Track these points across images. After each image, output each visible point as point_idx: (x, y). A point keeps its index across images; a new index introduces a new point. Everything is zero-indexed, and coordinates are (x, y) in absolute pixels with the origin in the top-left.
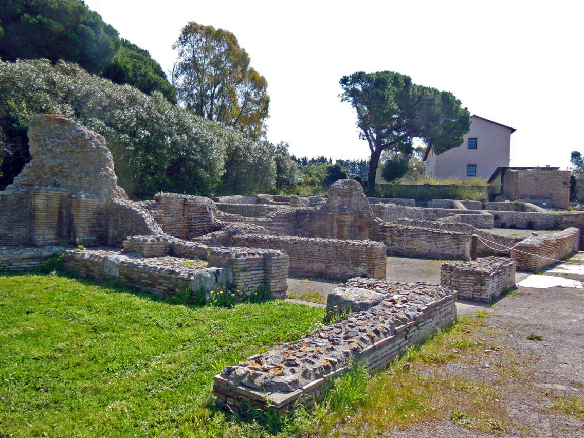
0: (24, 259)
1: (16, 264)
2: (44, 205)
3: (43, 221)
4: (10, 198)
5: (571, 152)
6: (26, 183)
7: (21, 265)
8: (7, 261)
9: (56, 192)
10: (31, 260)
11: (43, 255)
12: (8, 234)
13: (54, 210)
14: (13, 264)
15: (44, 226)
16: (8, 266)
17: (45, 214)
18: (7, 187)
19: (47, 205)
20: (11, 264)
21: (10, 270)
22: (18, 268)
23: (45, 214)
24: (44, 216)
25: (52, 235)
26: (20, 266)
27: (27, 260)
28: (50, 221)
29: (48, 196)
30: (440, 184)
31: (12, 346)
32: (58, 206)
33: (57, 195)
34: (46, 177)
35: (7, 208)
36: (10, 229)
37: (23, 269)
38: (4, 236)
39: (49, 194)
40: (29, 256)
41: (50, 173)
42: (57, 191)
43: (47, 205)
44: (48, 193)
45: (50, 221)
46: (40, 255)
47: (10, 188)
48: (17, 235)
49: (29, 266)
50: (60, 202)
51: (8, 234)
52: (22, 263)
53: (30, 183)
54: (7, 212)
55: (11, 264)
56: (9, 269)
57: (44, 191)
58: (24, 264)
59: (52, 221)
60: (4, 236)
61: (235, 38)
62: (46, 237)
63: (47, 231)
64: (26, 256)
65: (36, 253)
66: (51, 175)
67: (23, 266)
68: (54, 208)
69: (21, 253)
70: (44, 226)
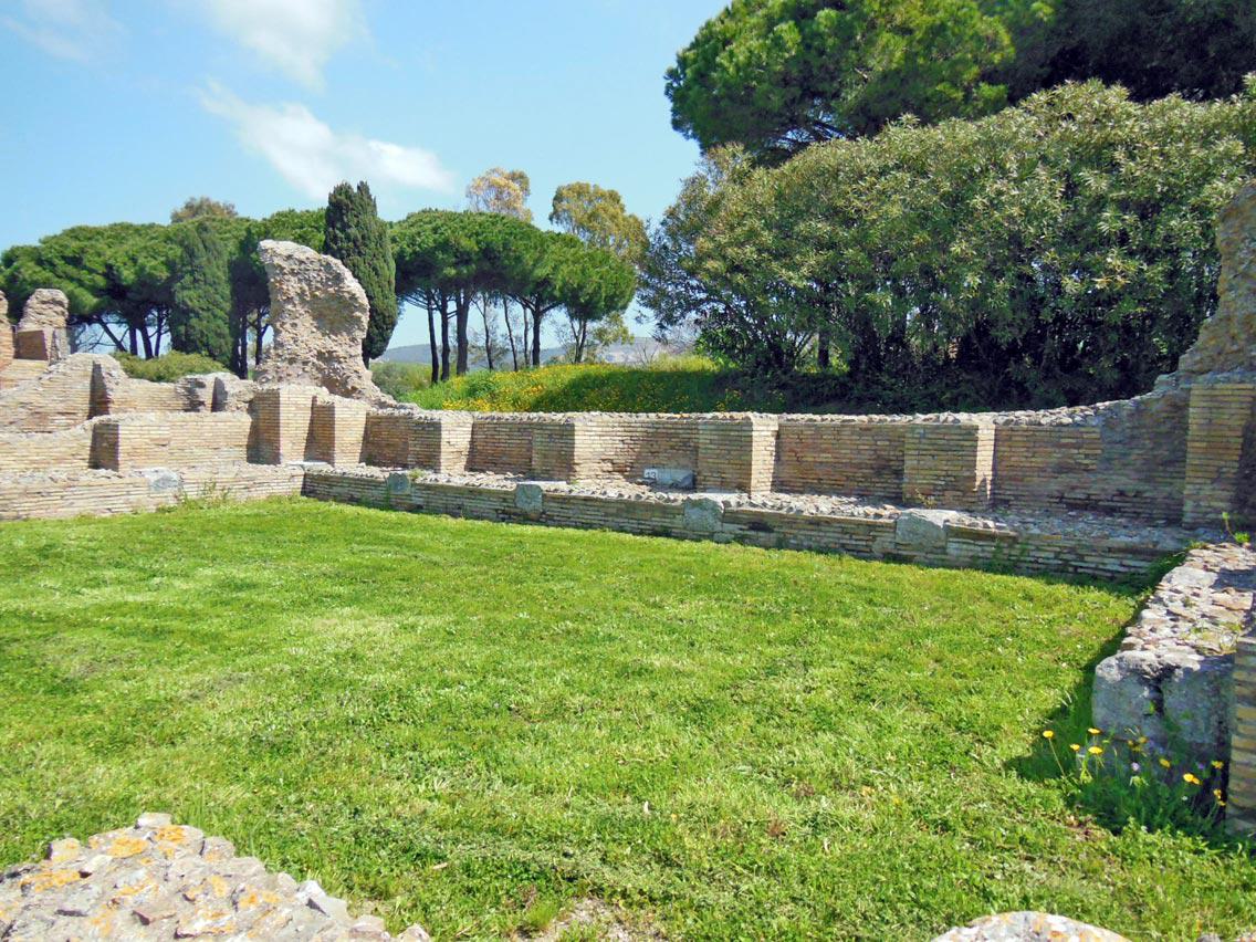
0: (1110, 550)
1: (1092, 560)
2: (1202, 421)
3: (1197, 462)
4: (1155, 407)
5: (557, 187)
6: (1196, 368)
7: (1104, 564)
8: (1072, 550)
9: (1241, 386)
10: (1130, 556)
11: (1159, 547)
12: (1146, 491)
13: (1228, 433)
14: (1086, 559)
15: (1200, 474)
16: (1075, 561)
17: (1204, 444)
18: (1156, 382)
19: (1210, 420)
20: (1081, 558)
21: (1080, 570)
22: (1096, 569)
23: (1204, 444)
24: (1200, 451)
25: (1222, 501)
26: (1101, 567)
27: (1120, 555)
28: (1216, 463)
29: (1213, 398)
30: (947, 416)
31: (370, 629)
32: (1243, 423)
33: (1243, 393)
34: (1235, 348)
35: (1144, 430)
36: (1148, 480)
37: (1109, 575)
38: (1135, 496)
39: (1217, 393)
40: (1123, 545)
41: (1243, 336)
42: (1241, 382)
43: (1210, 420)
44: (1213, 389)
45: (1216, 463)
46: (1151, 546)
47: (1162, 382)
48: (1165, 494)
49: (1122, 569)
50: (1249, 412)
51: (1146, 491)
52: (1106, 561)
53: (1206, 368)
54: (1145, 439)
55: (1081, 558)
56: (1076, 568)
57: (1200, 386)
58: (1112, 564)
59: (1223, 463)
60: (1135, 496)
61: (80, 228)
62: (1202, 504)
63: (1207, 490)
64: (1115, 545)
65: (1146, 540)
66: (1247, 340)
67: (1108, 567)
68: (1230, 429)
69: (1107, 537)
70: (1200, 474)
